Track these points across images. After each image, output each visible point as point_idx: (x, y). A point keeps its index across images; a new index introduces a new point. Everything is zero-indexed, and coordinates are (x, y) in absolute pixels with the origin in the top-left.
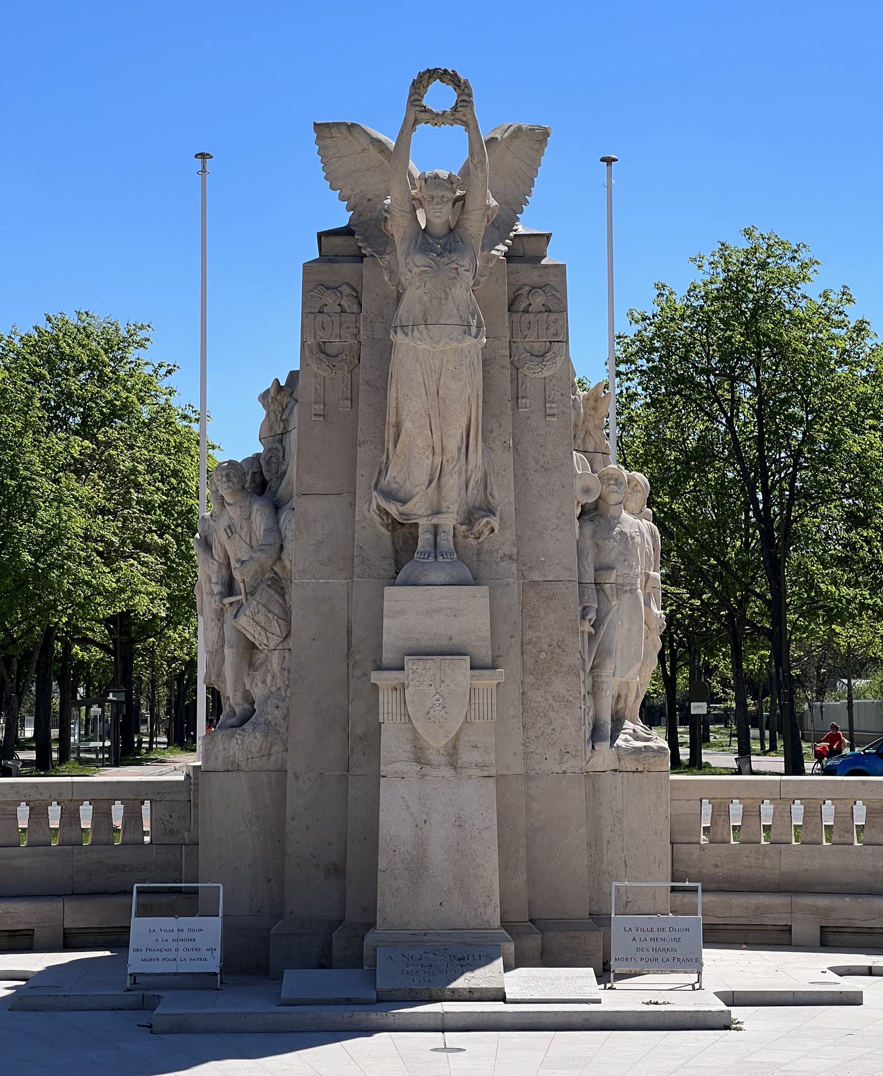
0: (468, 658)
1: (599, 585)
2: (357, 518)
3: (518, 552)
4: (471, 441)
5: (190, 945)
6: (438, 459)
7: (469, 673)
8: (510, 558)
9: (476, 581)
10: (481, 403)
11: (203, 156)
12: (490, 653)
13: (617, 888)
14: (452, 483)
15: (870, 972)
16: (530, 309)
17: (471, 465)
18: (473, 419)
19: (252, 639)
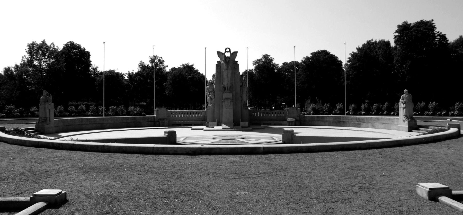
9: (231, 92)
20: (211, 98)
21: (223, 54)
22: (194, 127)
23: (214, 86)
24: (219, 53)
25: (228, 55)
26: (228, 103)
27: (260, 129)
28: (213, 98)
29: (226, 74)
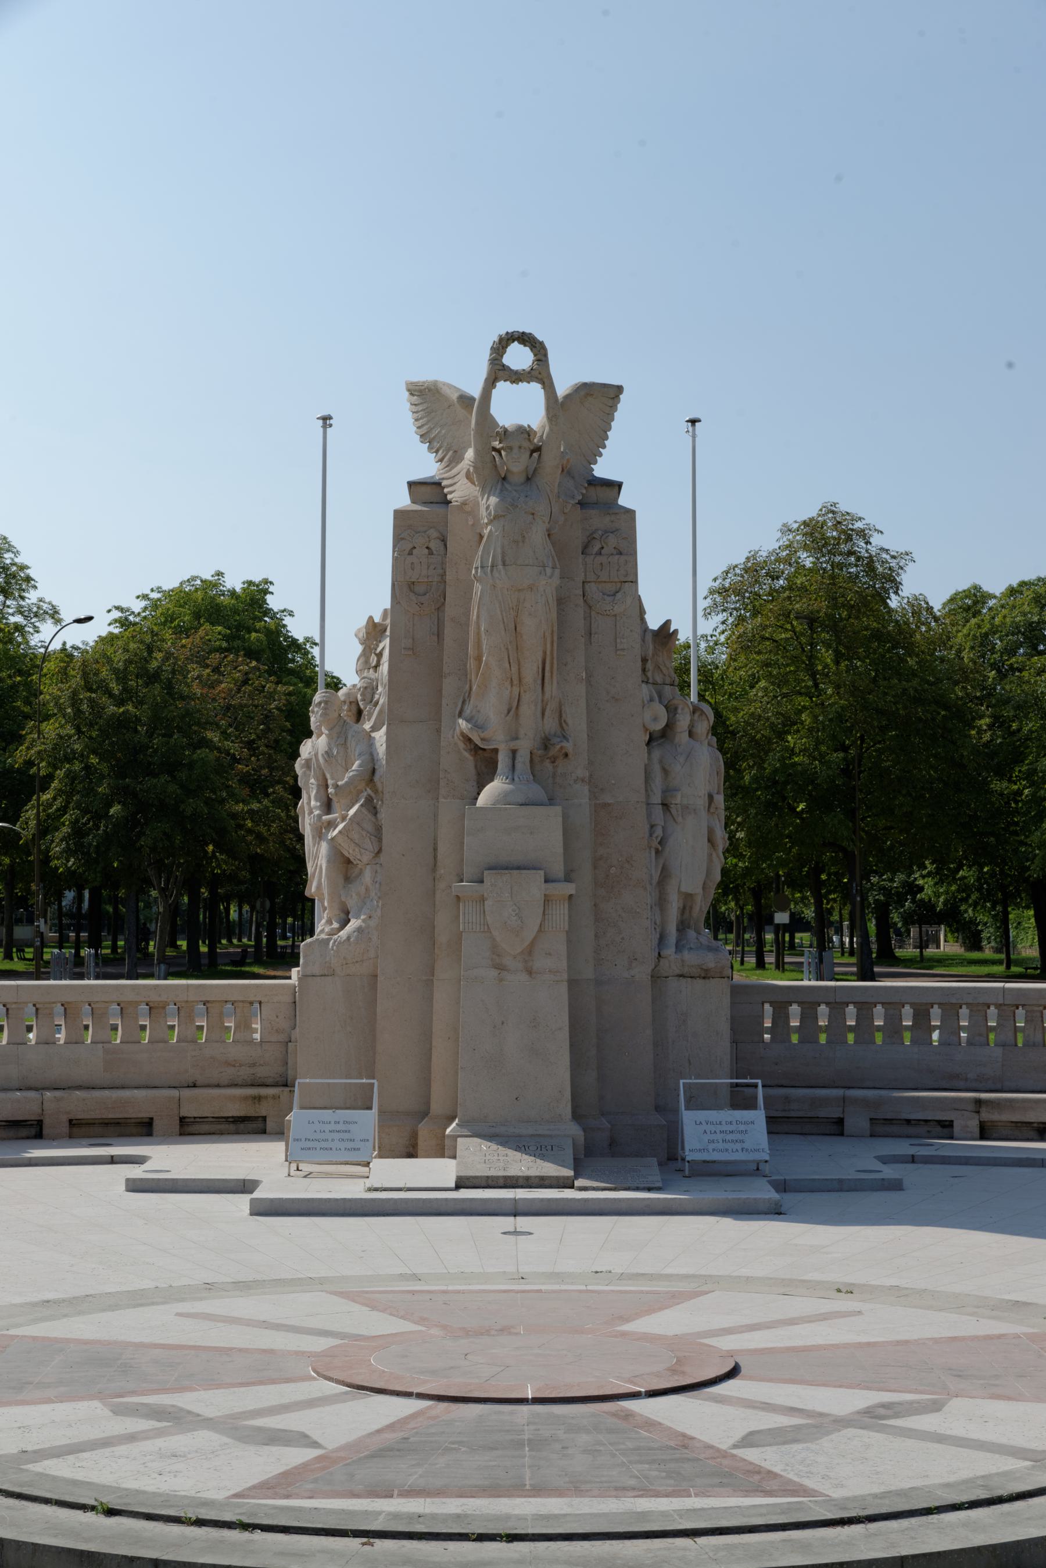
0: (542, 873)
1: (665, 805)
2: (442, 744)
3: (591, 776)
4: (547, 674)
5: (346, 1136)
6: (516, 690)
7: (543, 886)
8: (583, 781)
9: (551, 801)
10: (555, 638)
11: (693, 422)
12: (562, 868)
13: (756, 1086)
14: (528, 711)
15: (913, 1159)
16: (603, 551)
17: (547, 695)
18: (548, 653)
19: (346, 854)
20: (345, 867)
21: (466, 400)
22: (169, 1158)
23: (380, 737)
24: (427, 398)
25: (519, 407)
26: (518, 906)
27: (841, 1186)
28: (362, 857)
29: (498, 601)
